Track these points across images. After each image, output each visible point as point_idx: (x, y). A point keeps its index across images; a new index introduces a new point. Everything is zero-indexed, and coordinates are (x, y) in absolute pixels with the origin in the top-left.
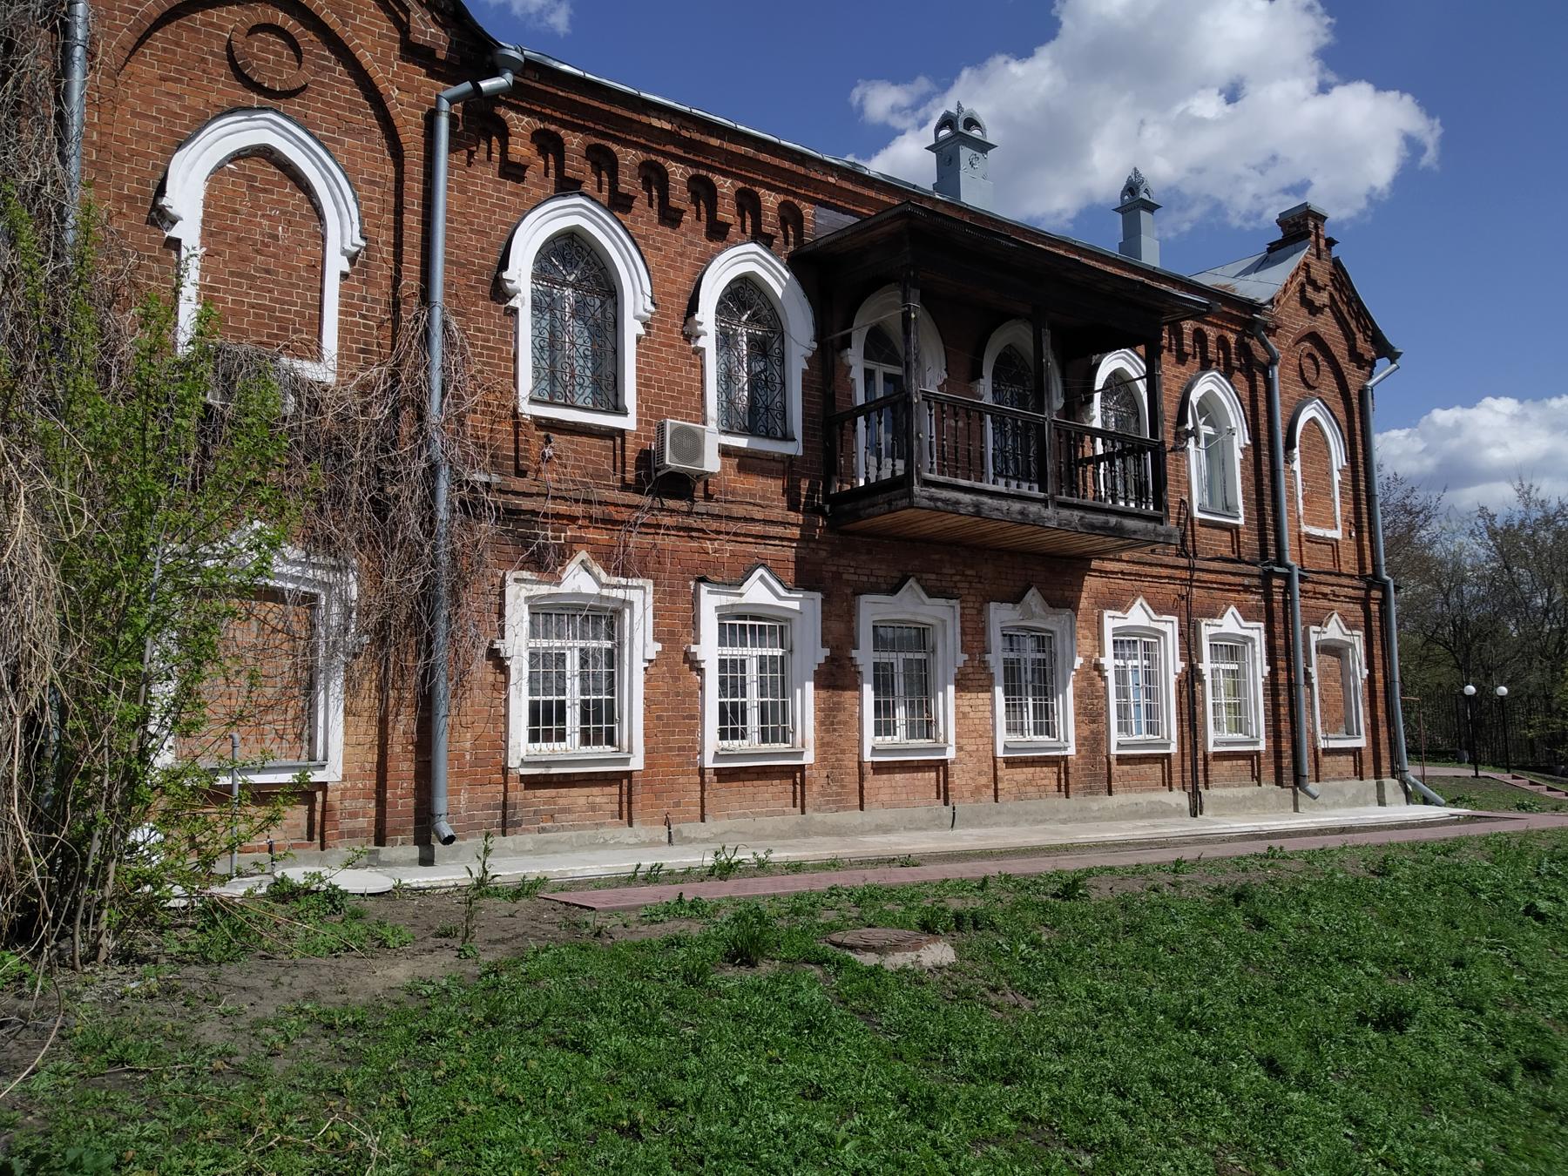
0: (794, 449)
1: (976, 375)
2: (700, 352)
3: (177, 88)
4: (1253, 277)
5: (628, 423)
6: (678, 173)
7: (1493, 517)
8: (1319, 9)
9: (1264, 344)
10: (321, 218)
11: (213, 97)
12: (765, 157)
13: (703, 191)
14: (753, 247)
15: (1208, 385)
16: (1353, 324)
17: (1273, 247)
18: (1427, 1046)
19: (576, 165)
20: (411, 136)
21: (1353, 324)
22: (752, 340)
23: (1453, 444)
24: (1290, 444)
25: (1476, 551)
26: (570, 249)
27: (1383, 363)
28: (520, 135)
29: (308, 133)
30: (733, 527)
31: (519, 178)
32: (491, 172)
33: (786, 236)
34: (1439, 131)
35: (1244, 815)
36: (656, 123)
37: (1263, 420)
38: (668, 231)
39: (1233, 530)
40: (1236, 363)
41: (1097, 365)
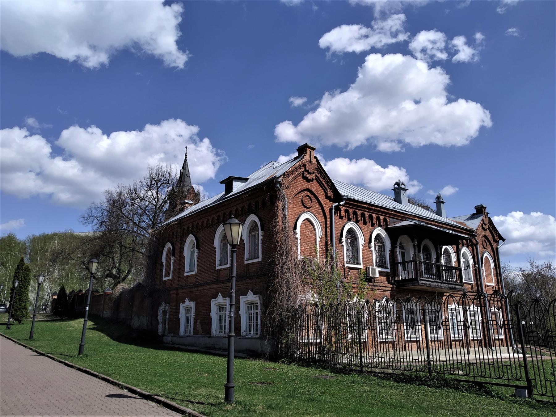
1: (419, 252)
3: (295, 209)
7: (524, 271)
8: (442, 72)
9: (475, 240)
10: (315, 230)
11: (300, 210)
14: (380, 228)
17: (474, 214)
20: (328, 213)
25: (519, 280)
26: (350, 231)
27: (501, 241)
30: (381, 288)
31: (342, 219)
35: (475, 355)
36: (364, 206)
37: (476, 258)
39: (471, 284)
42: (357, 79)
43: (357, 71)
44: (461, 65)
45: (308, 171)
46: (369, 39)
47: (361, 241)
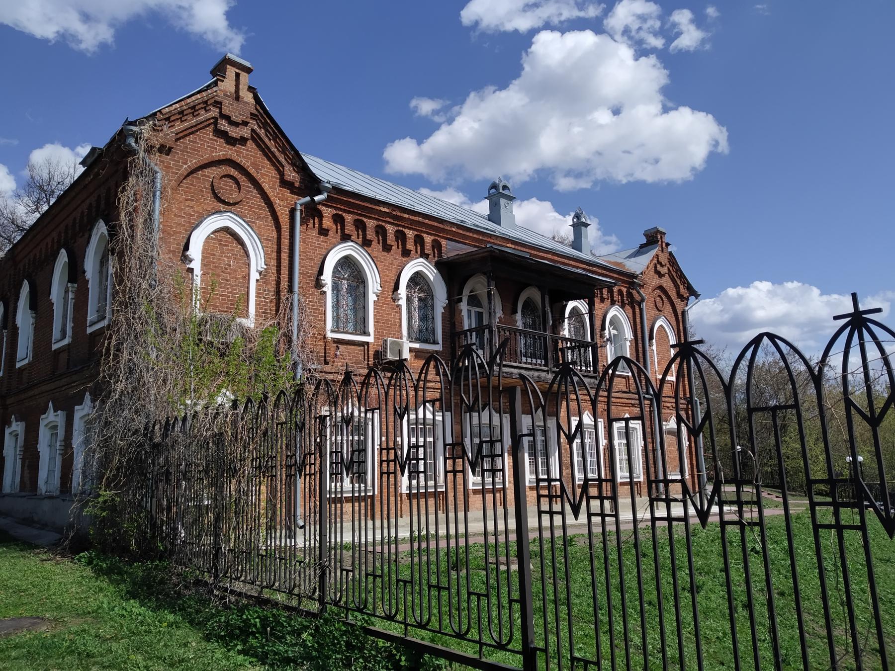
0: (439, 348)
1: (515, 312)
2: (399, 306)
3: (191, 203)
4: (633, 259)
5: (370, 339)
6: (391, 229)
8: (659, 65)
9: (638, 293)
10: (248, 256)
11: (206, 207)
12: (426, 221)
13: (401, 236)
14: (421, 260)
15: (614, 311)
16: (678, 281)
17: (642, 246)
18: (708, 598)
19: (350, 228)
20: (284, 220)
21: (678, 281)
22: (420, 299)
23: (738, 307)
24: (651, 338)
26: (347, 262)
27: (692, 298)
28: (327, 217)
29: (244, 221)
31: (326, 235)
32: (315, 233)
33: (434, 253)
34: (726, 134)
36: (382, 209)
37: (639, 327)
38: (386, 254)
40: (626, 302)
41: (566, 305)
42: (523, 73)
43: (521, 59)
44: (683, 54)
45: (227, 118)
46: (540, 9)
47: (374, 284)
